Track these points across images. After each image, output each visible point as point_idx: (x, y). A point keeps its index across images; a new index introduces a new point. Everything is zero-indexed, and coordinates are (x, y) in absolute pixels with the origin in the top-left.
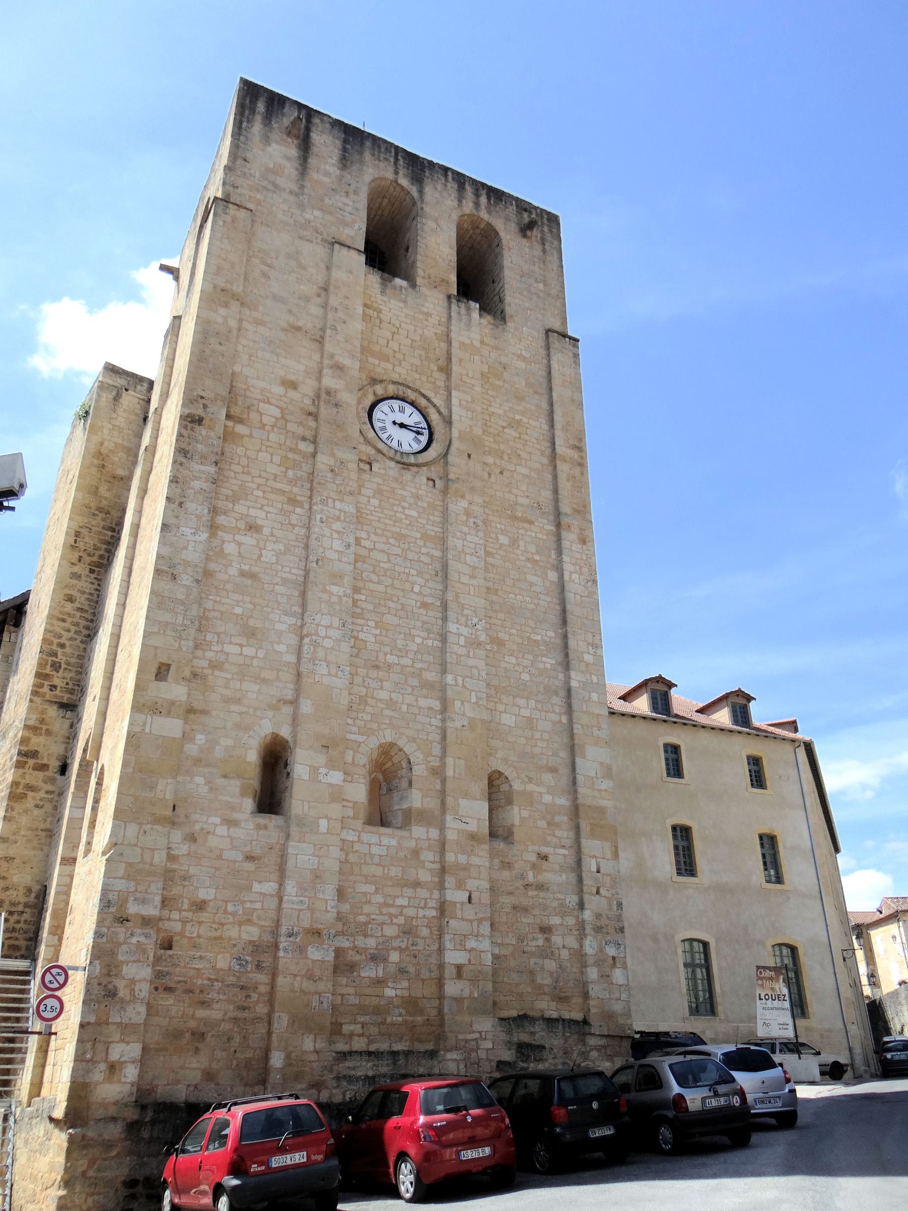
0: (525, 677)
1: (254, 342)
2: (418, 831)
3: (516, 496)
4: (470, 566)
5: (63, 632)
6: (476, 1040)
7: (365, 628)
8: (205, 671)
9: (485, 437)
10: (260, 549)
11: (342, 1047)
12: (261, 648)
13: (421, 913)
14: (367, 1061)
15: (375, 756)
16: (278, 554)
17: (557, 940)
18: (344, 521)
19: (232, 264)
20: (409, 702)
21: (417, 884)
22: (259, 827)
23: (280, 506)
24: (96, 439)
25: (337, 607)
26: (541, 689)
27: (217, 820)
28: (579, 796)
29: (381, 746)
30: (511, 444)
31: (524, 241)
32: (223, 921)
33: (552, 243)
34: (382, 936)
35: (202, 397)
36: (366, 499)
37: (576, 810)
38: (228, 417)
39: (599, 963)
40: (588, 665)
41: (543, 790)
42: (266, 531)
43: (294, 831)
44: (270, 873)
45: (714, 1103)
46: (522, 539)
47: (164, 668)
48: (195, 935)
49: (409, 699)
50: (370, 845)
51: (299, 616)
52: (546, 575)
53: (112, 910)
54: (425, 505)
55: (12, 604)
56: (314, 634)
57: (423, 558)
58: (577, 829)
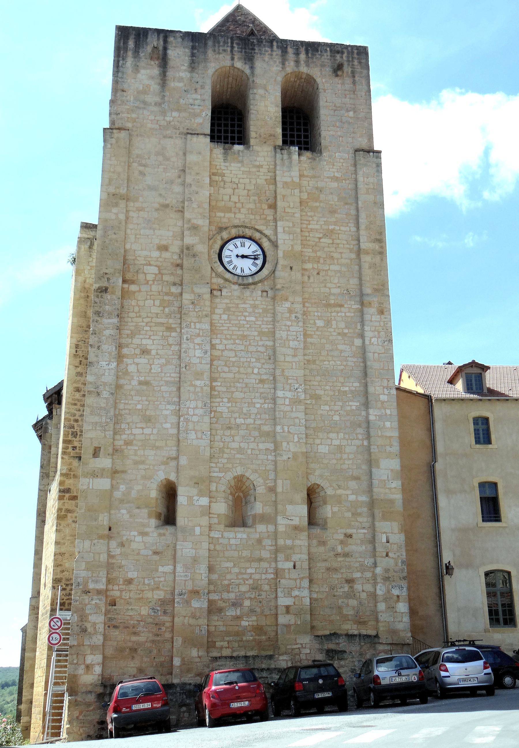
0: (336, 418)
1: (138, 224)
2: (261, 528)
3: (330, 288)
4: (292, 348)
5: (75, 412)
6: (299, 648)
7: (221, 404)
8: (122, 447)
9: (304, 250)
10: (151, 365)
11: (215, 654)
12: (155, 428)
13: (264, 577)
14: (231, 661)
15: (233, 484)
16: (162, 366)
17: (358, 587)
18: (203, 336)
19: (119, 174)
20: (252, 447)
21: (260, 560)
22: (160, 535)
23: (161, 334)
24: (81, 279)
25: (200, 394)
26: (348, 424)
27: (136, 533)
28: (374, 494)
29: (235, 478)
30: (326, 249)
31: (337, 80)
32: (143, 589)
33: (361, 73)
34: (239, 591)
35: (106, 274)
36: (219, 316)
37: (372, 504)
38: (124, 281)
39: (386, 599)
40: (383, 402)
41: (349, 492)
42: (153, 352)
43: (180, 535)
44: (169, 560)
45: (398, 680)
46: (335, 320)
47: (97, 450)
48: (128, 597)
49: (253, 445)
50: (229, 539)
51: (177, 404)
52: (353, 343)
53: (81, 587)
54: (261, 311)
55: (54, 391)
56: (186, 415)
57: (260, 349)
58: (373, 516)
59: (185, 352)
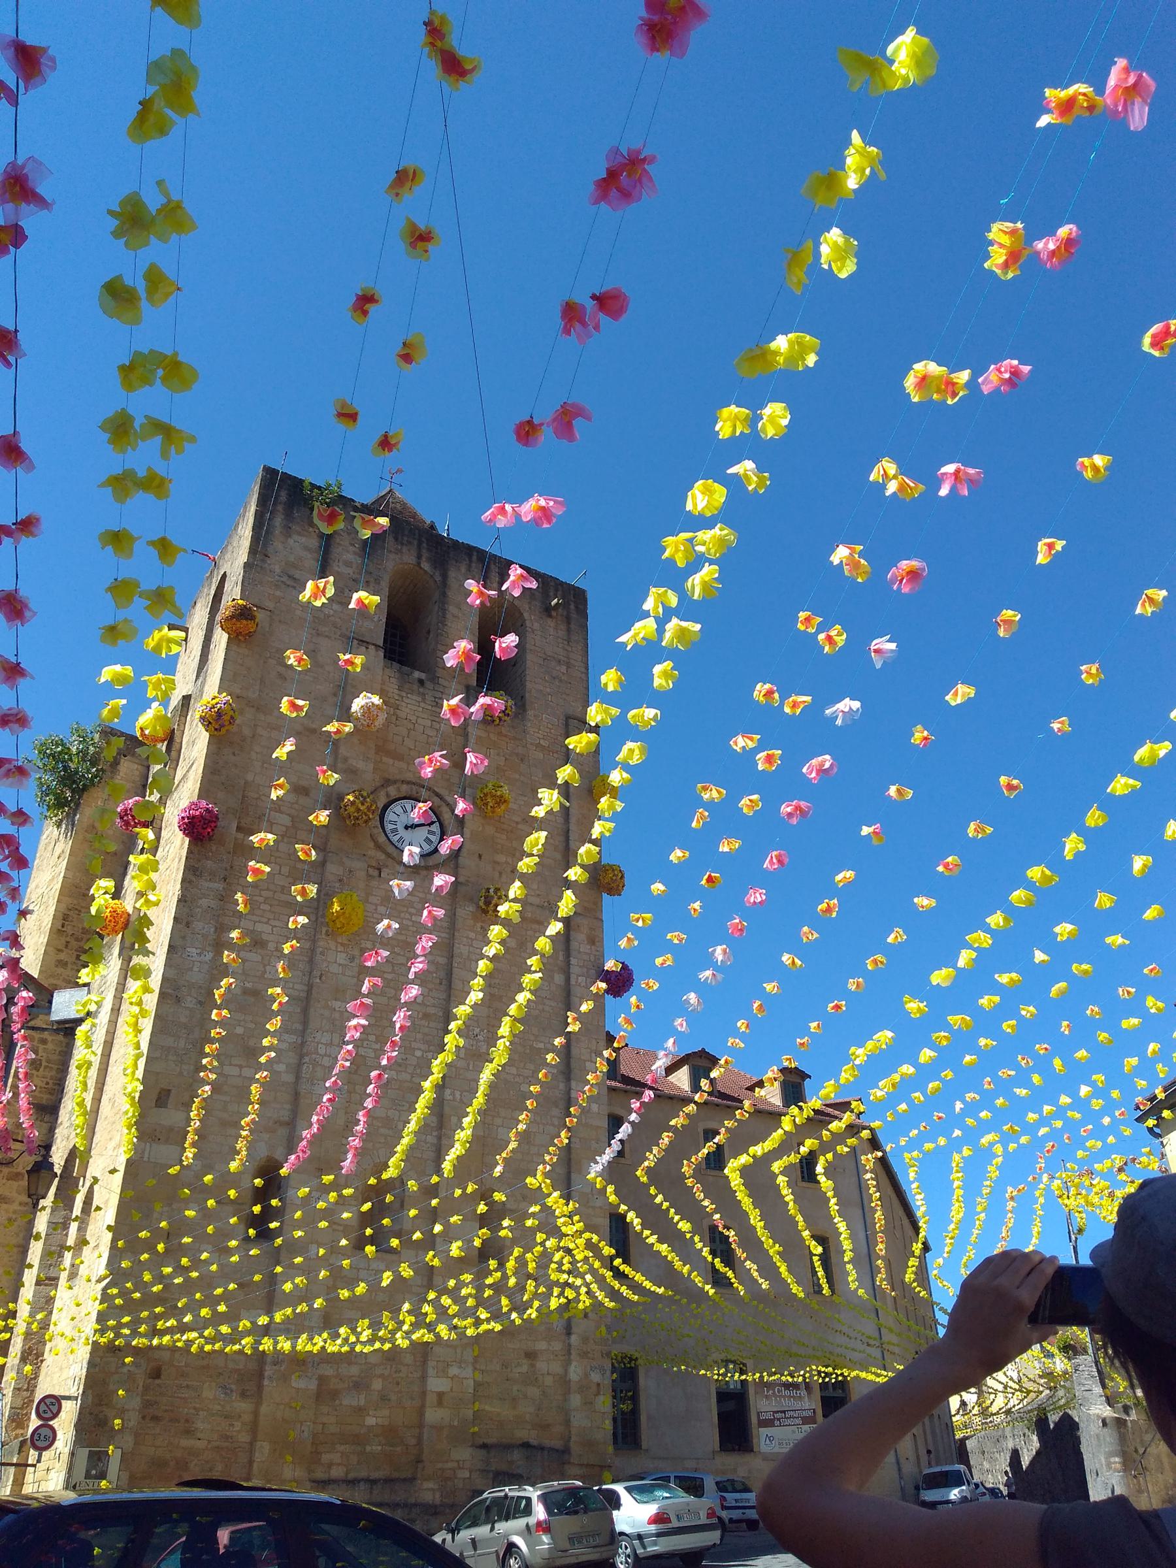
10: (265, 966)
17: (542, 1366)
48: (183, 1364)
59: (322, 953)
